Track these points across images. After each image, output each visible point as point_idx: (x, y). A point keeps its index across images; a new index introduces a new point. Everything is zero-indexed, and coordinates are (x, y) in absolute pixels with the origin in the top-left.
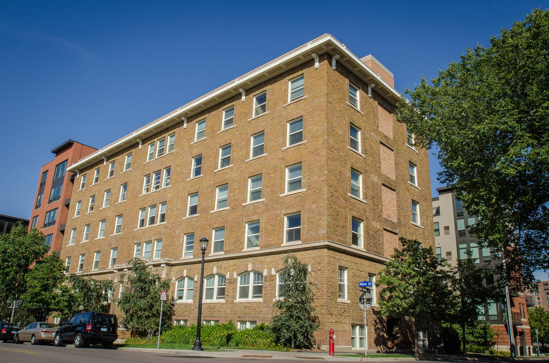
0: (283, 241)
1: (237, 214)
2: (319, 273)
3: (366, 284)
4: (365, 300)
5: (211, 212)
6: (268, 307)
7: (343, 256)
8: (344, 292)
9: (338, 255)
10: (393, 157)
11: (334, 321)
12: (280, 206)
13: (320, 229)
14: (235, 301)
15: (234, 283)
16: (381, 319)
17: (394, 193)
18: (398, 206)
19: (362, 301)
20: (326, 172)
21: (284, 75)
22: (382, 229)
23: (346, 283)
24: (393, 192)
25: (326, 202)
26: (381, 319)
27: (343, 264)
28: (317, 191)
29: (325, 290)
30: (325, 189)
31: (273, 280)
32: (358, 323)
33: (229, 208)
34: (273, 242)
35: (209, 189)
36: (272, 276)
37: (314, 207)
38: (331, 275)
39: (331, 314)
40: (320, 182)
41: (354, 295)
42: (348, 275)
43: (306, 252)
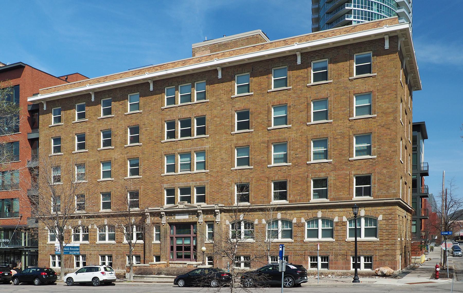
1: (300, 170)
28: (388, 159)
34: (343, 196)
37: (385, 171)
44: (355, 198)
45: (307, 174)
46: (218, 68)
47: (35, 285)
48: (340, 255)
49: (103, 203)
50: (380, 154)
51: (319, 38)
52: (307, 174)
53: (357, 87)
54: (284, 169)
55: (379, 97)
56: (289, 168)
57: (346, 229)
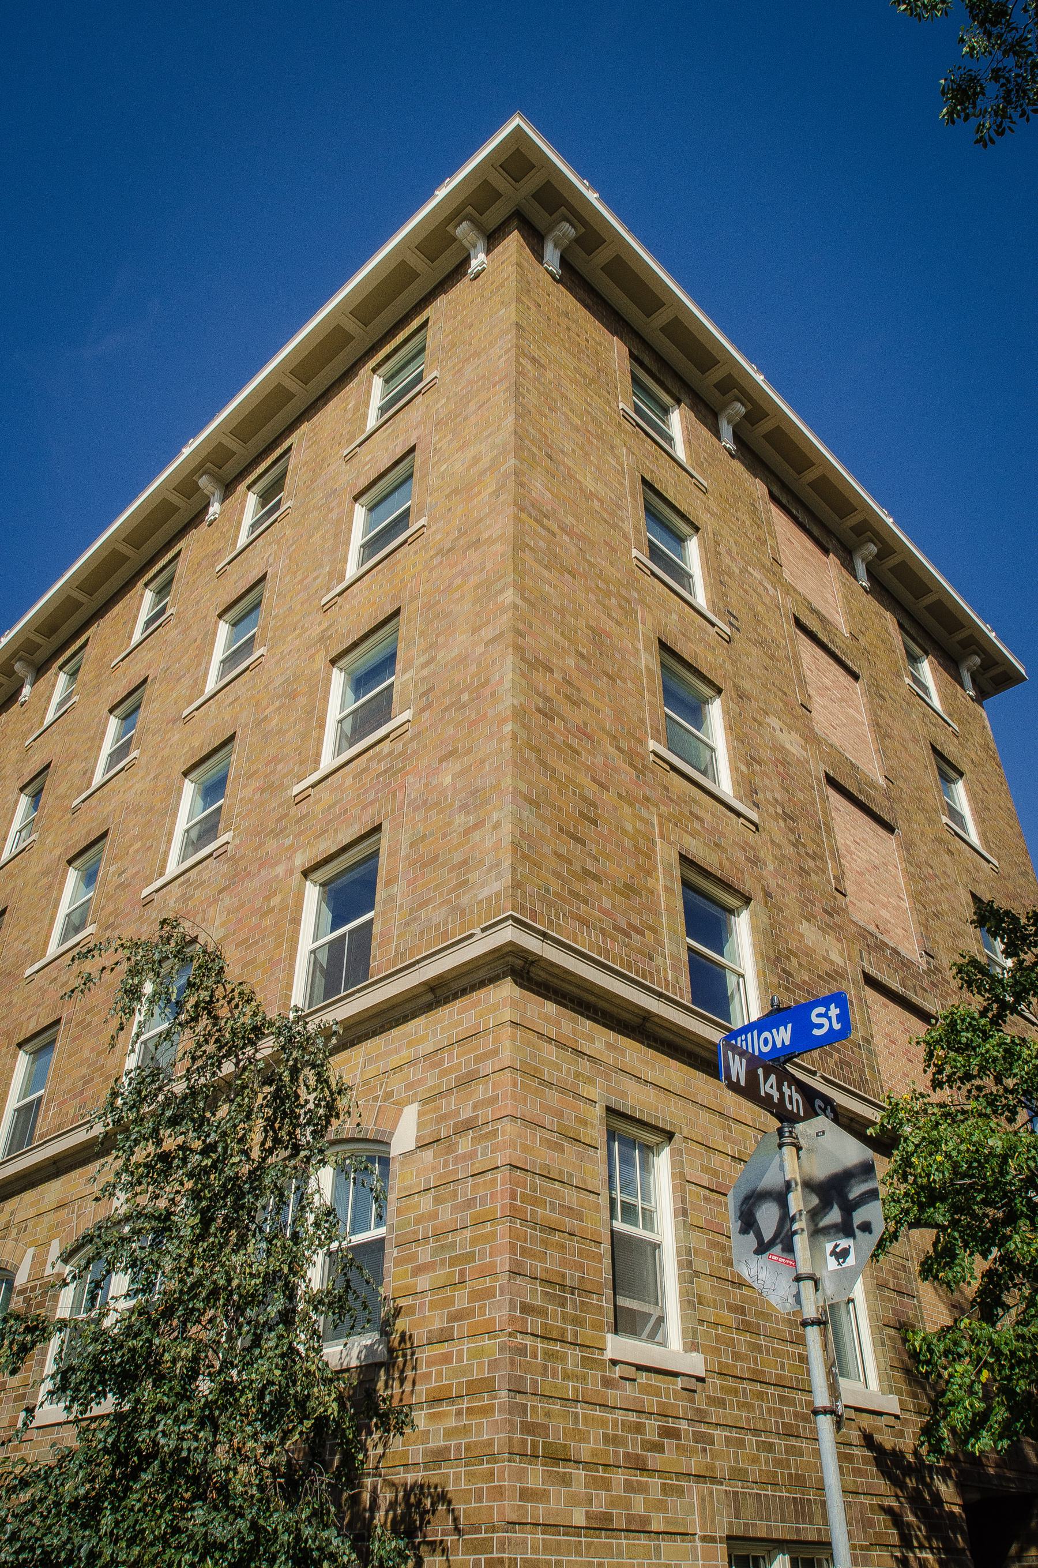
2: (464, 1144)
3: (783, 1036)
4: (796, 1202)
7: (635, 1054)
8: (655, 1297)
9: (598, 1039)
10: (861, 701)
11: (579, 1518)
12: (288, 841)
13: (474, 876)
16: (929, 1509)
17: (891, 842)
18: (918, 897)
19: (768, 1216)
20: (509, 596)
22: (854, 973)
23: (666, 1232)
24: (882, 832)
25: (508, 728)
26: (929, 1509)
27: (638, 1100)
29: (503, 1262)
30: (506, 671)
32: (780, 1530)
38: (547, 1157)
39: (557, 1457)
40: (480, 649)
41: (731, 1319)
42: (681, 1181)
43: (395, 1032)
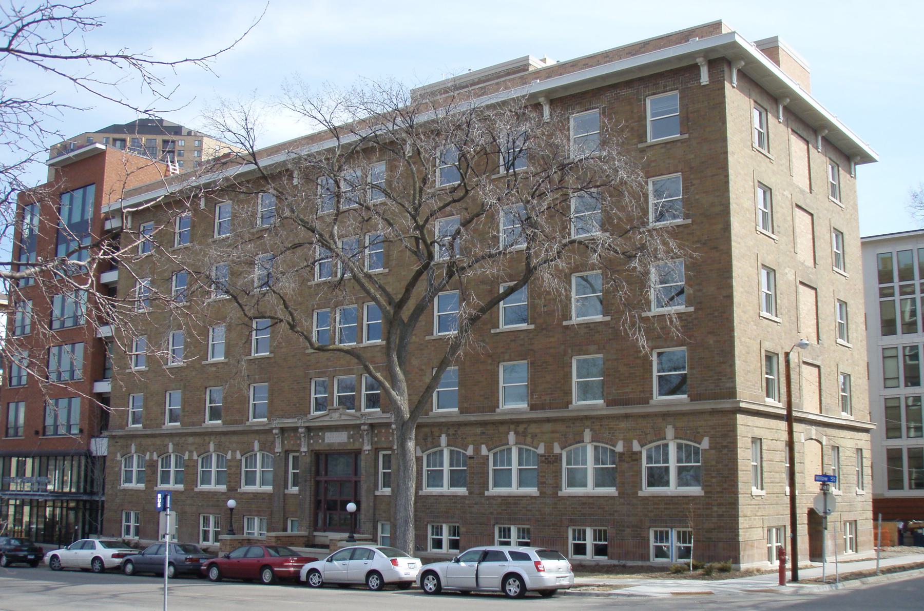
0: (652, 394)
1: (552, 339)
2: (725, 451)
5: (493, 331)
6: (628, 504)
14: (560, 494)
15: (556, 462)
21: (662, 82)
28: (716, 314)
31: (636, 460)
33: (532, 327)
34: (631, 396)
35: (485, 287)
36: (636, 453)
37: (711, 340)
44: (658, 398)
45: (563, 347)
46: (700, 60)
47: (263, 583)
48: (628, 527)
49: (660, 377)
50: (700, 303)
51: (582, 69)
52: (563, 347)
53: (653, 164)
54: (522, 337)
55: (694, 182)
56: (531, 336)
57: (641, 468)
